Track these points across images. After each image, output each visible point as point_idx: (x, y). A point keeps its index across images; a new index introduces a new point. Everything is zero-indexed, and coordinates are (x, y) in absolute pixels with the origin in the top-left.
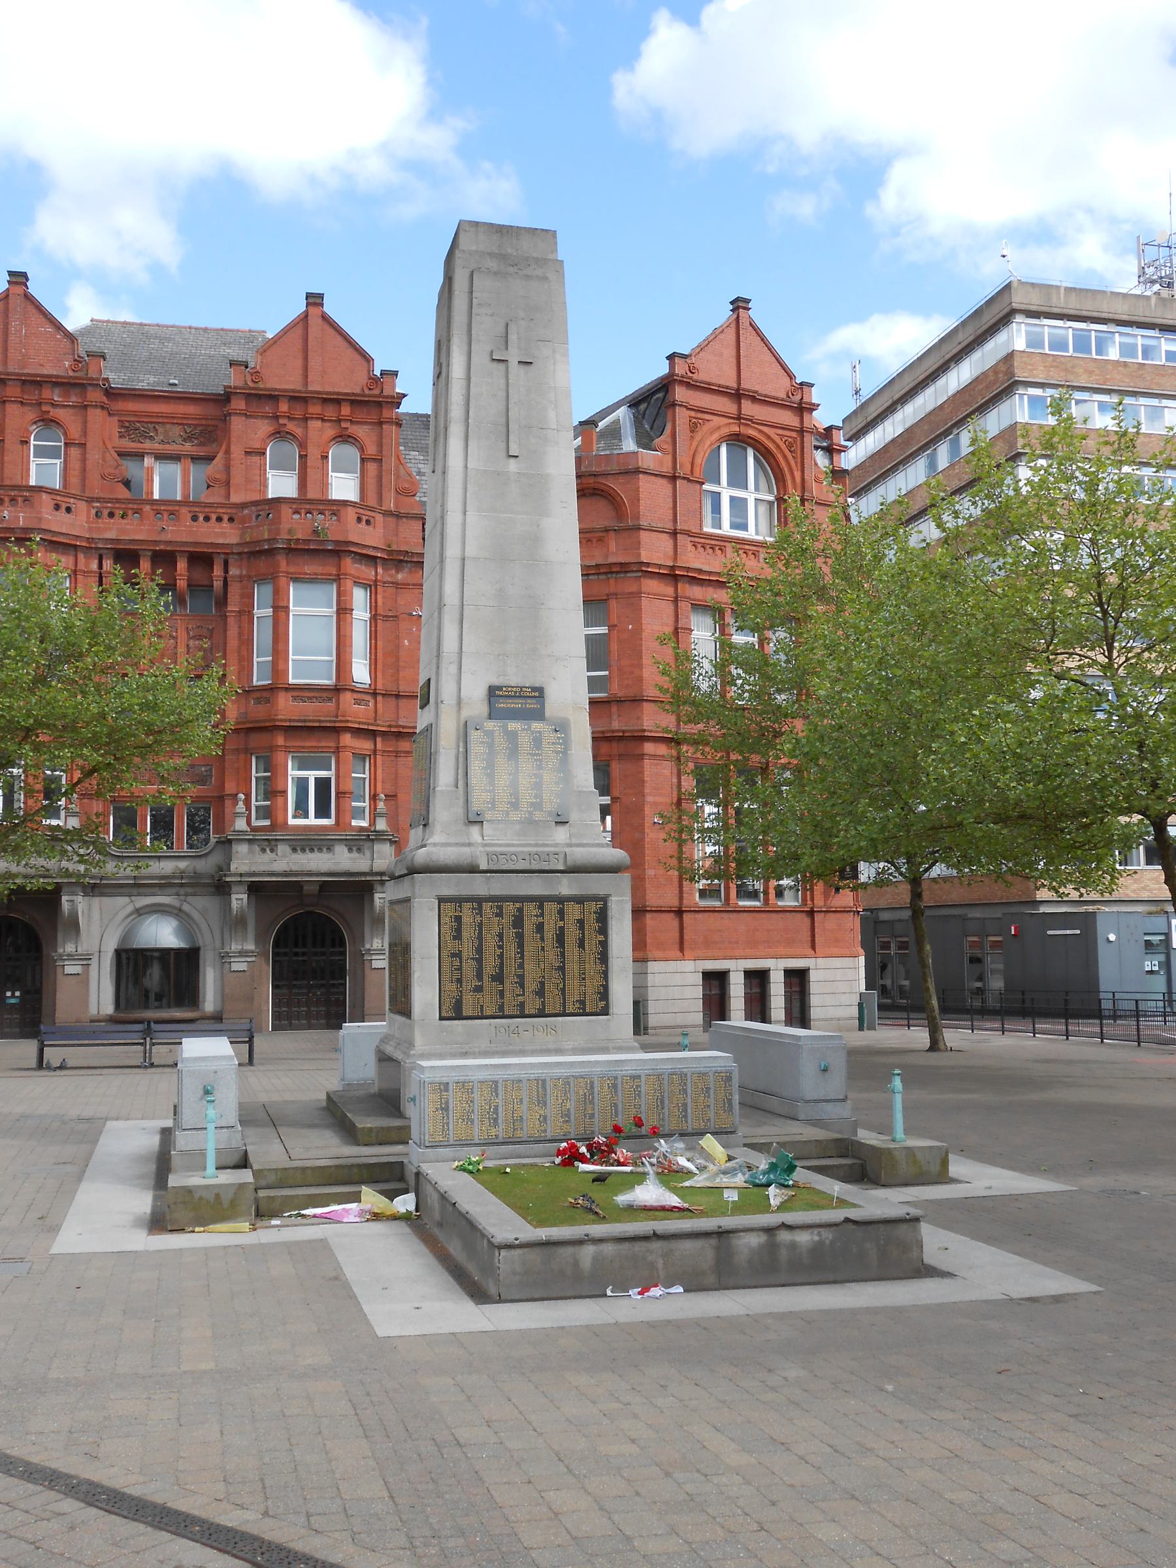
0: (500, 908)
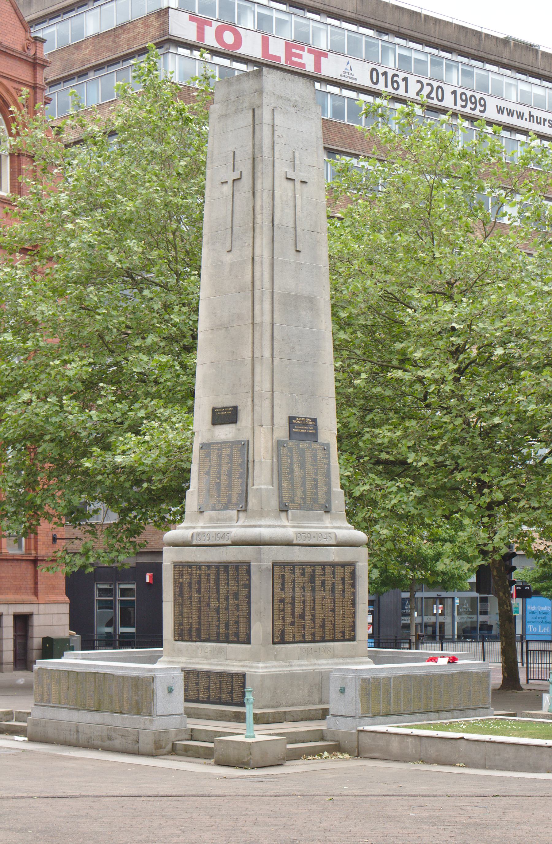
0: (304, 569)
